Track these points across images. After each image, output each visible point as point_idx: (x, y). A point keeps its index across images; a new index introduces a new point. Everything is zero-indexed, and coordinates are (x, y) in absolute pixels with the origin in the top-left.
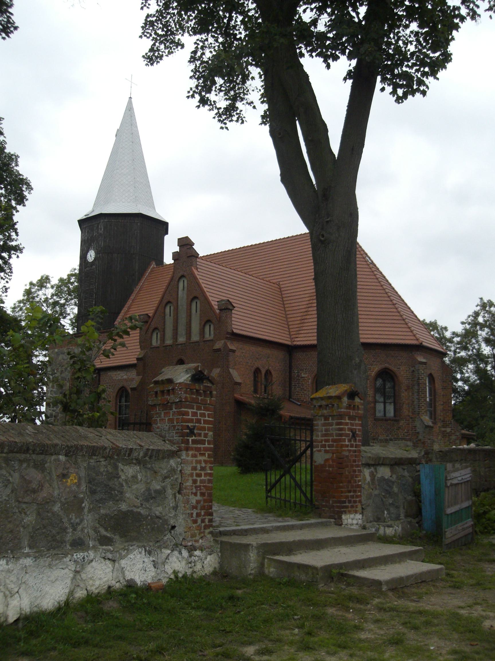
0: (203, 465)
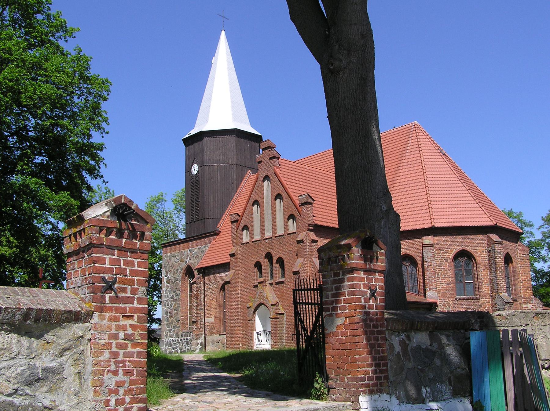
0: (130, 331)
